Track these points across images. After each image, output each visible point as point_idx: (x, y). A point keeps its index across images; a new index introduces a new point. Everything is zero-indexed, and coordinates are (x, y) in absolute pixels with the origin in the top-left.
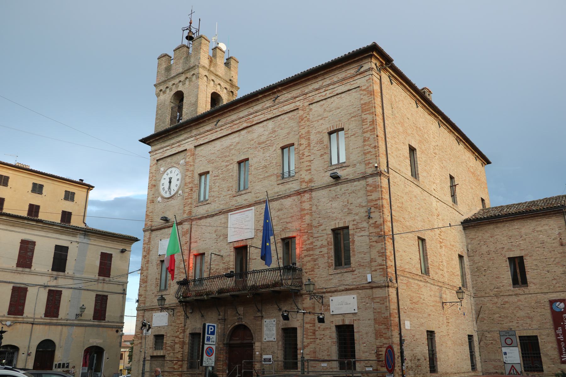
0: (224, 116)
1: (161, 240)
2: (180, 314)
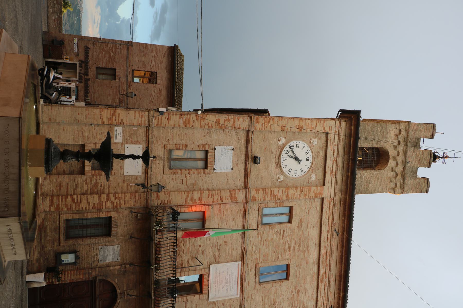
1: (233, 149)
2: (137, 199)
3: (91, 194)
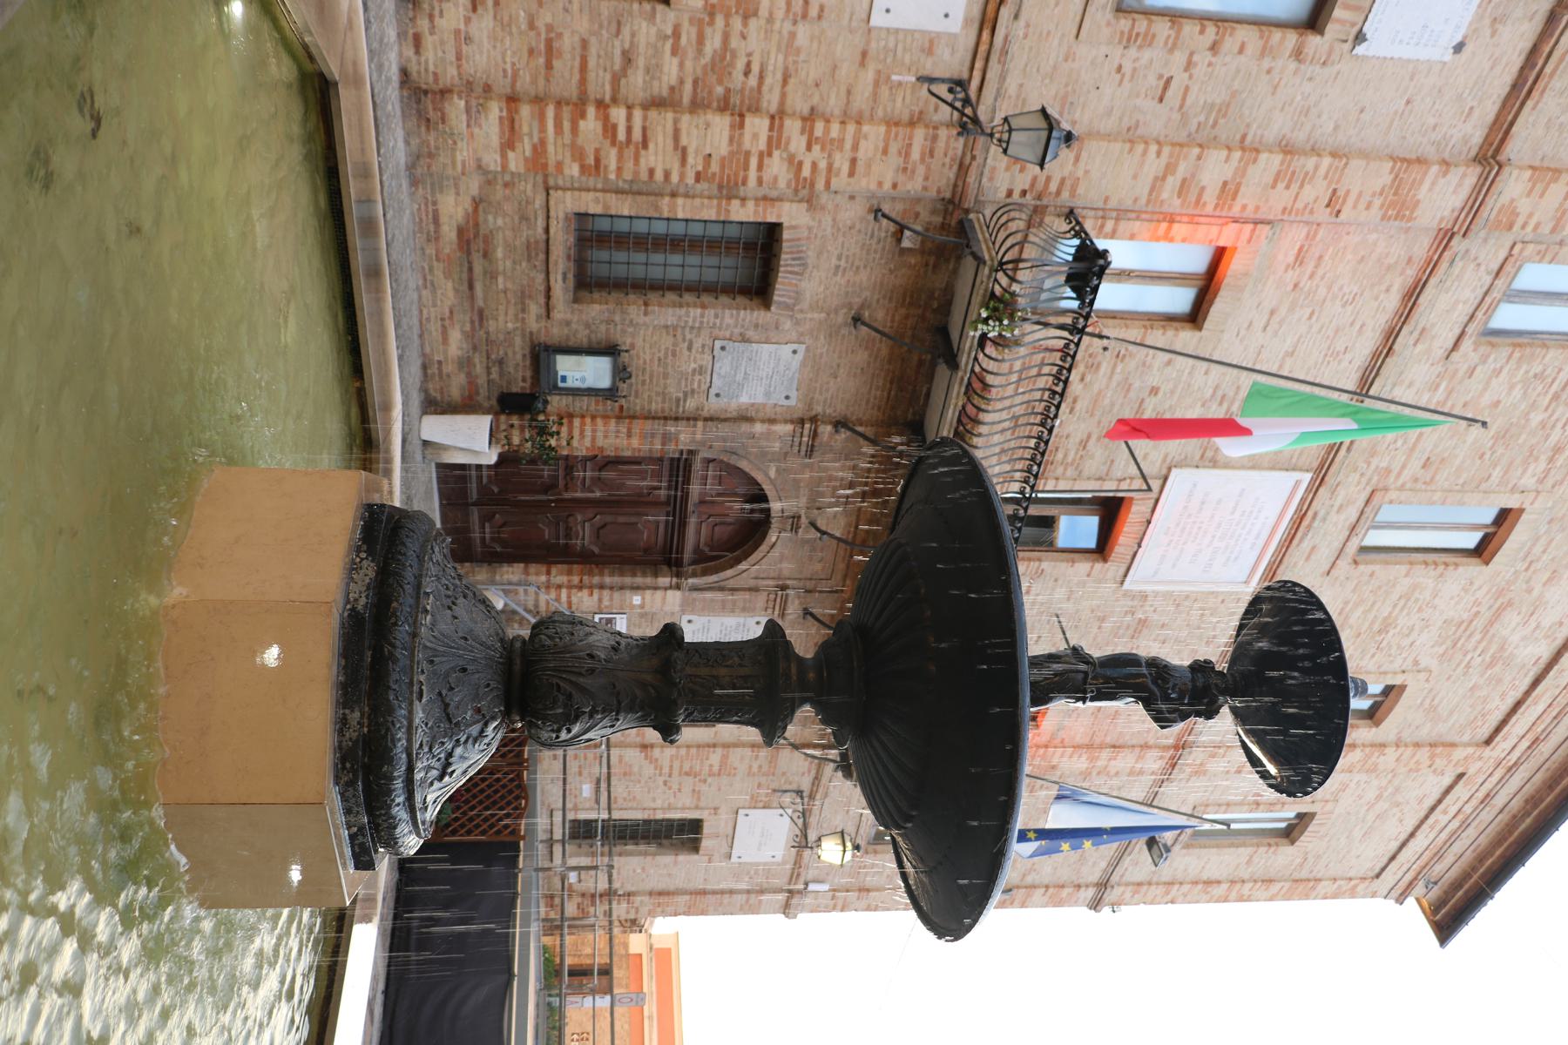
2: (916, 154)
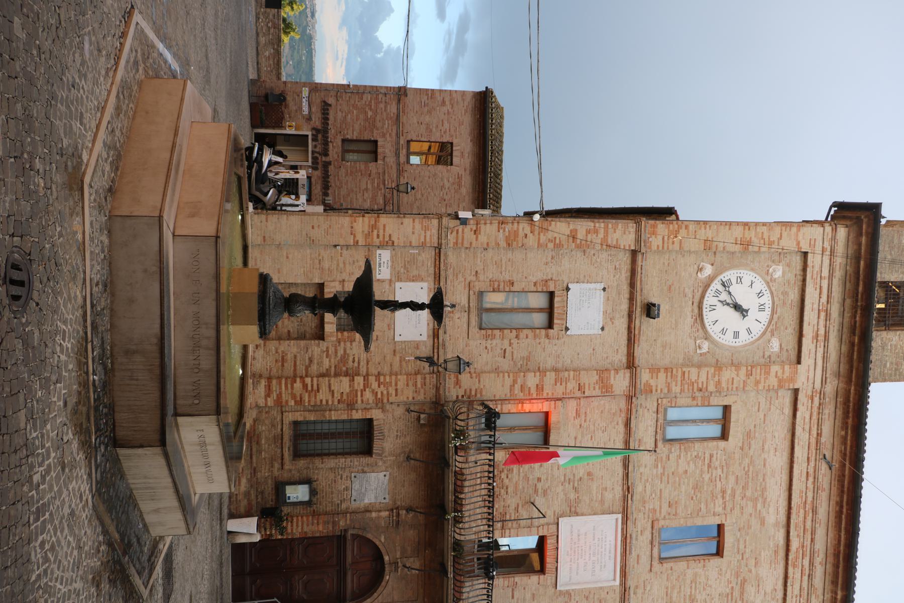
0: (835, 483)
1: (604, 289)
2: (419, 385)
3: (336, 375)
